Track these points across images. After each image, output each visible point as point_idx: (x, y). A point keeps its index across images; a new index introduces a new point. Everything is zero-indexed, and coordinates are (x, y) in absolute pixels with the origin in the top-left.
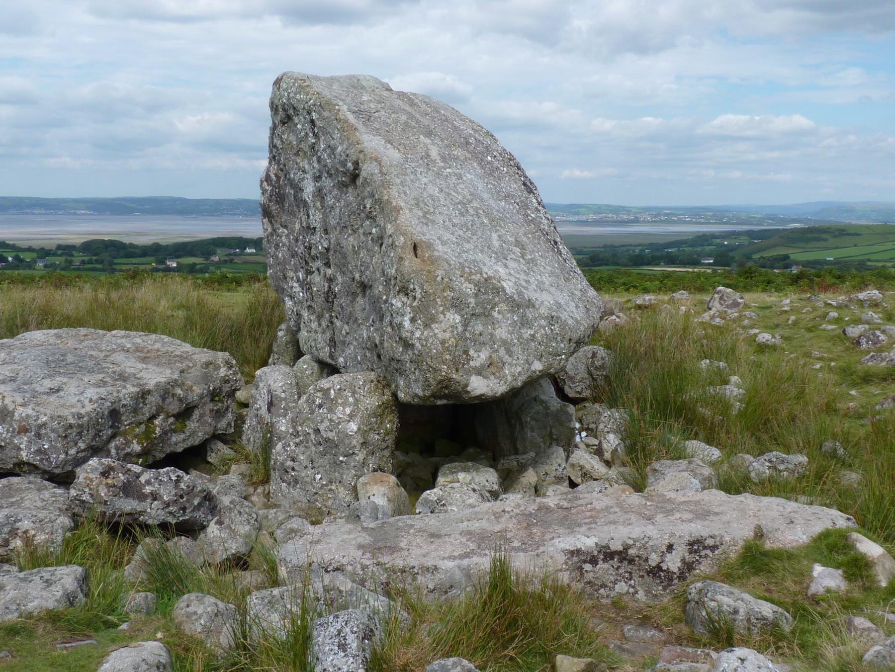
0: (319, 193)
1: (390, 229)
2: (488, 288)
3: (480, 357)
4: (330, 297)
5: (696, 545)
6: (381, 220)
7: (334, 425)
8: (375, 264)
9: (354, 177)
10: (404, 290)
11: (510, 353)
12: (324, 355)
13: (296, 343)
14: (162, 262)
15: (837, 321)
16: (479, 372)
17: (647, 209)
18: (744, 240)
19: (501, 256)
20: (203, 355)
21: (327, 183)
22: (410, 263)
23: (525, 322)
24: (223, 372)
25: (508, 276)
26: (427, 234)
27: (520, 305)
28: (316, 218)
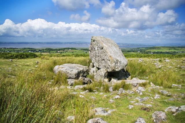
0: (98, 49)
1: (107, 54)
2: (117, 60)
3: (117, 67)
4: (99, 60)
5: (137, 84)
6: (106, 53)
7: (102, 74)
8: (105, 58)
9: (102, 48)
10: (109, 61)
11: (119, 67)
12: (98, 67)
13: (93, 65)
14: (57, 51)
15: (153, 62)
16: (117, 69)
17: (130, 44)
18: (144, 48)
19: (118, 57)
20: (85, 67)
21: (99, 48)
22: (110, 58)
23: (121, 64)
24: (87, 68)
25: (119, 59)
26: (111, 55)
27: (120, 62)
28: (97, 52)
